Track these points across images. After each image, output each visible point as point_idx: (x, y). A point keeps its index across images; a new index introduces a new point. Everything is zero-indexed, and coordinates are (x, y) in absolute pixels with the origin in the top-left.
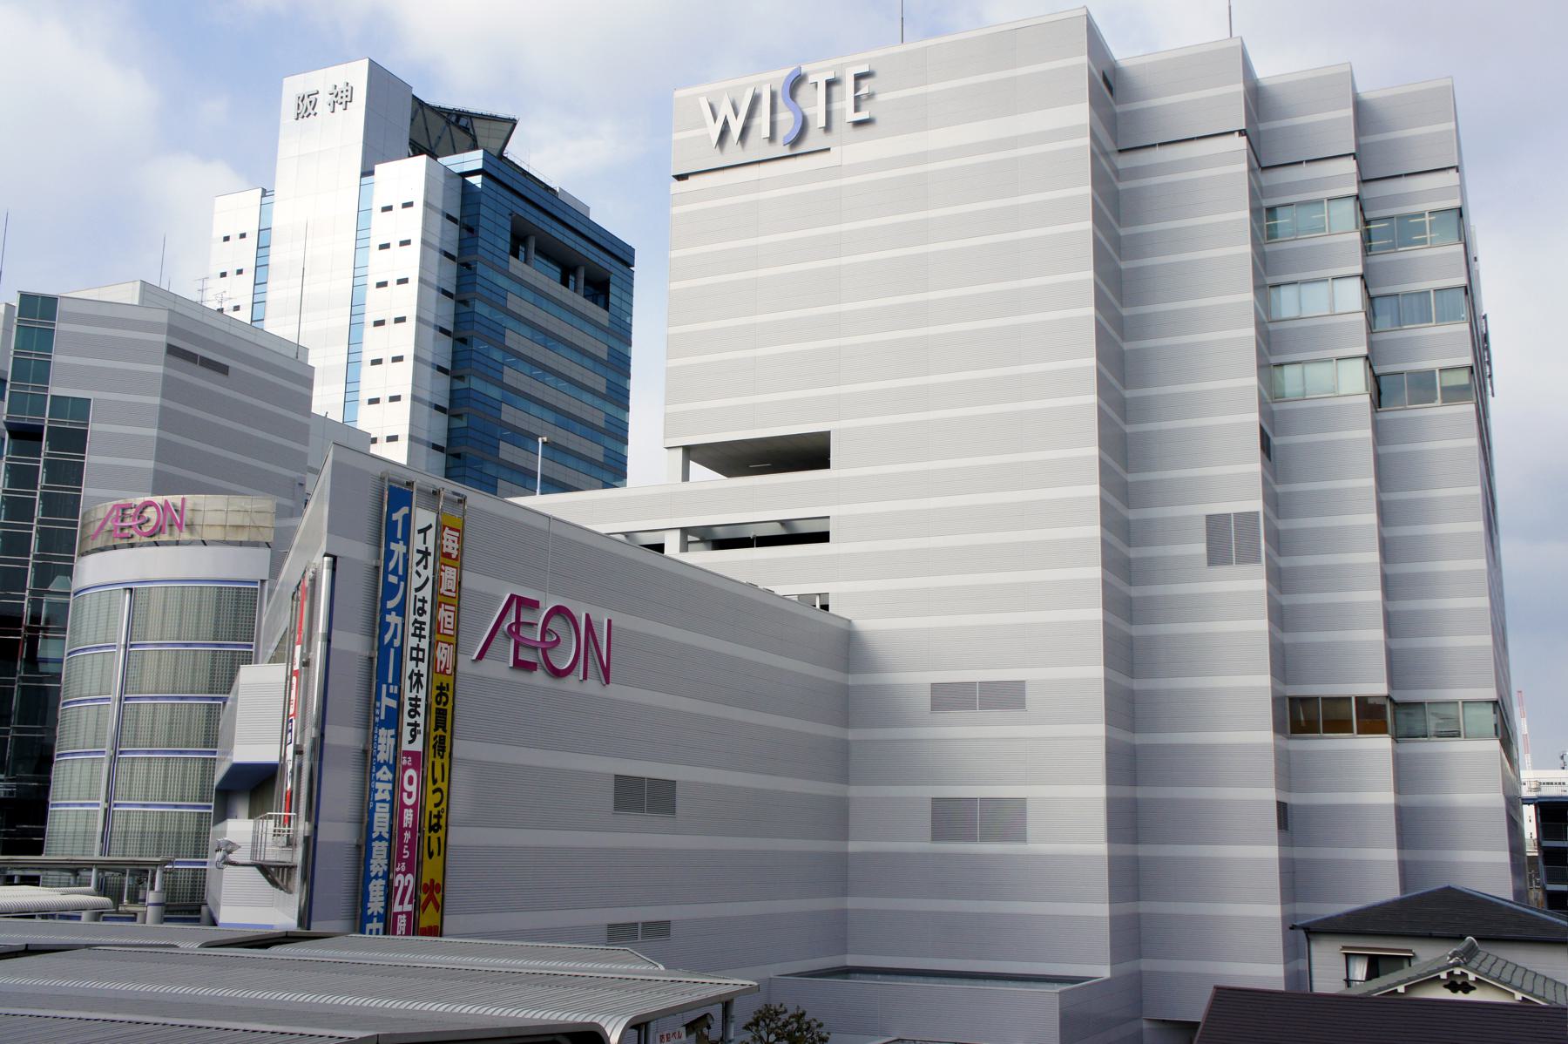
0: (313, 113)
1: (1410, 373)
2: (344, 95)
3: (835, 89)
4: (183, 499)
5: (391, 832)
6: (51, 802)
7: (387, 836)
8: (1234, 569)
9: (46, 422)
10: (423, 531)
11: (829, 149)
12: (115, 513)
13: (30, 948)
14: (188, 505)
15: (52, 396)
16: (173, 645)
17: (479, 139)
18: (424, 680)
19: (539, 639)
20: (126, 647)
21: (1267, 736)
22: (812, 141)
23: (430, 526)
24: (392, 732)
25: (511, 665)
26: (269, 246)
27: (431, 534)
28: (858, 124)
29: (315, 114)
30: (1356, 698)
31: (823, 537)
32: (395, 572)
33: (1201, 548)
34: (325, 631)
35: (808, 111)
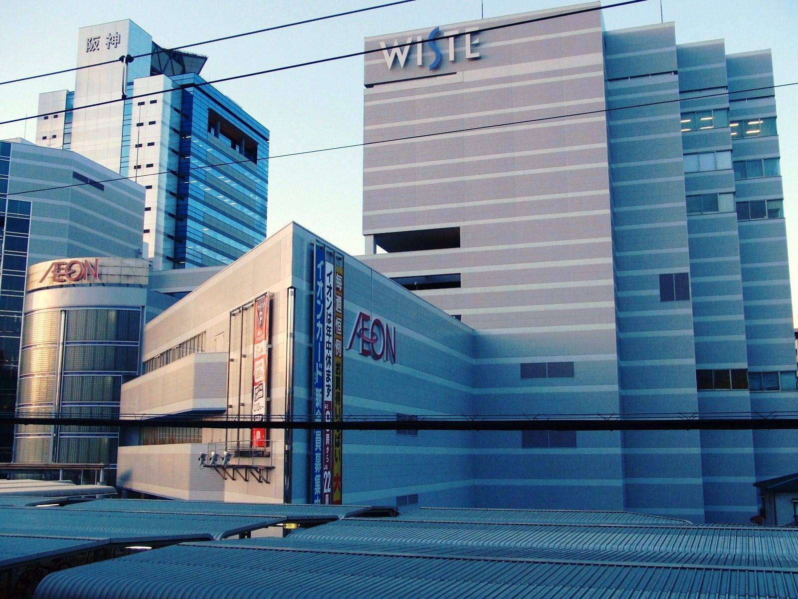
0: (97, 48)
1: (752, 202)
2: (115, 39)
4: (97, 260)
5: (322, 447)
6: (15, 434)
7: (320, 449)
8: (676, 303)
9: (6, 215)
10: (329, 275)
11: (455, 73)
12: (54, 267)
13: (289, 519)
14: (99, 262)
15: (9, 200)
16: (92, 343)
18: (331, 360)
19: (370, 338)
20: (63, 344)
21: (694, 390)
23: (331, 273)
24: (320, 390)
25: (361, 352)
27: (332, 276)
29: (98, 49)
30: (732, 370)
31: (457, 284)
32: (319, 298)
33: (657, 292)
34: (292, 331)
35: (443, 52)
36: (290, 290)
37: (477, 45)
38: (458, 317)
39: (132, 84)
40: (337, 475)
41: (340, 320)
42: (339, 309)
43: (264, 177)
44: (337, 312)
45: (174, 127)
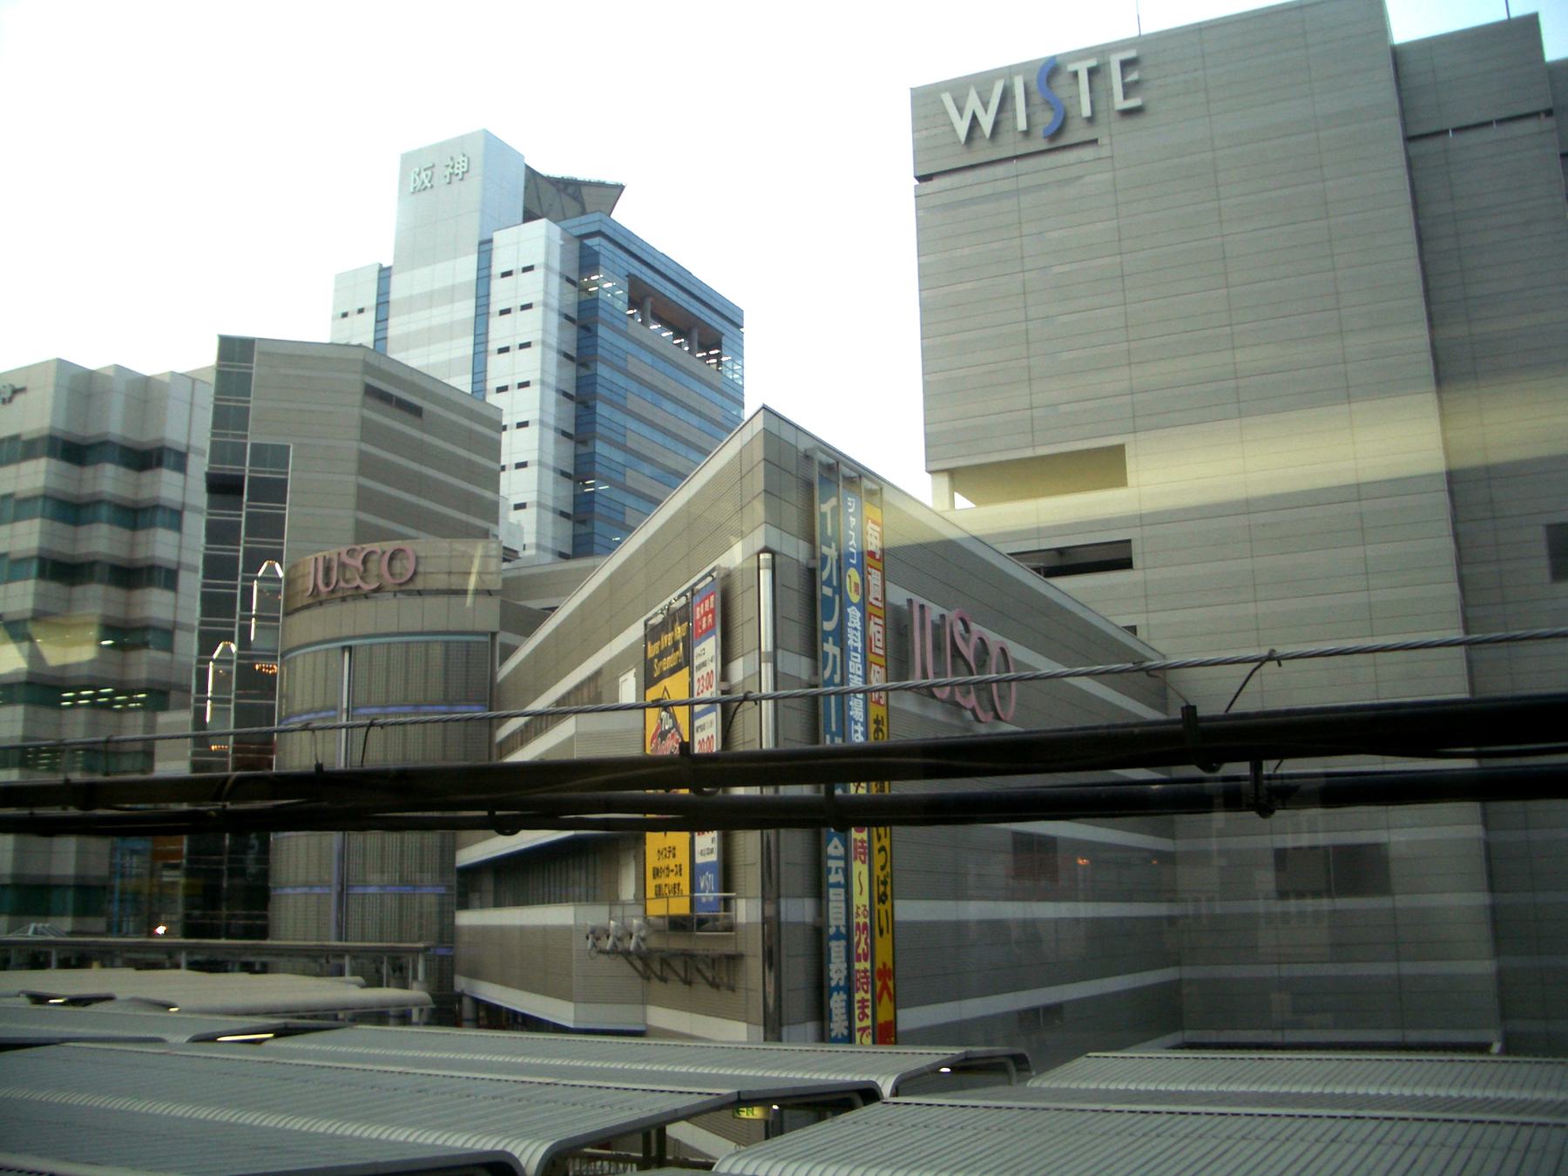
0: (429, 185)
3: (1098, 81)
9: (247, 471)
13: (742, 1097)
17: (587, 205)
22: (1076, 133)
26: (387, 320)
28: (1128, 113)
31: (1125, 564)
32: (828, 583)
36: (762, 556)
37: (1136, 83)
38: (1133, 630)
39: (491, 241)
40: (884, 965)
41: (881, 622)
42: (877, 599)
43: (737, 396)
44: (871, 604)
45: (566, 311)
